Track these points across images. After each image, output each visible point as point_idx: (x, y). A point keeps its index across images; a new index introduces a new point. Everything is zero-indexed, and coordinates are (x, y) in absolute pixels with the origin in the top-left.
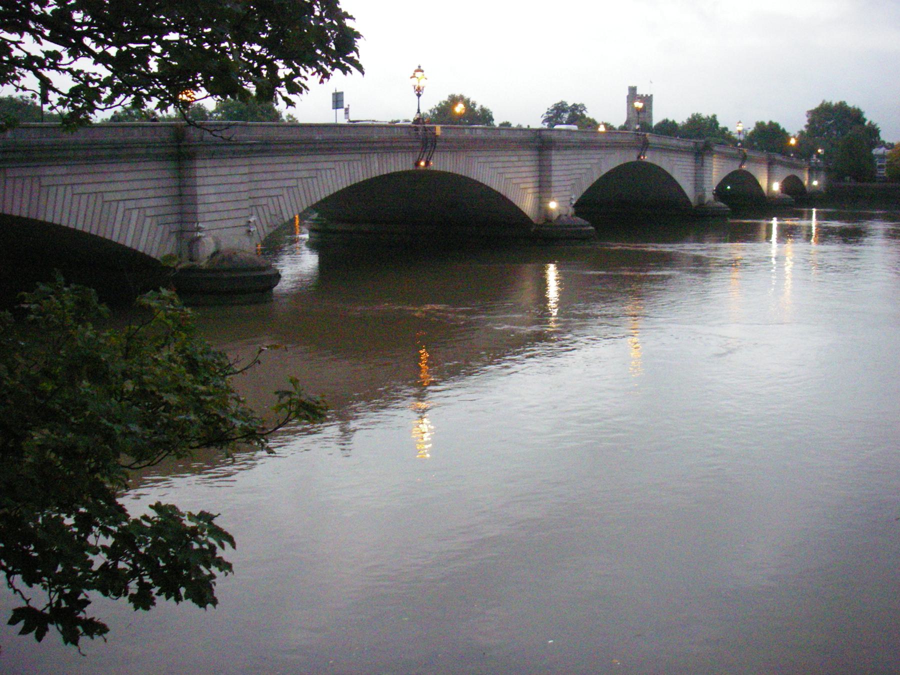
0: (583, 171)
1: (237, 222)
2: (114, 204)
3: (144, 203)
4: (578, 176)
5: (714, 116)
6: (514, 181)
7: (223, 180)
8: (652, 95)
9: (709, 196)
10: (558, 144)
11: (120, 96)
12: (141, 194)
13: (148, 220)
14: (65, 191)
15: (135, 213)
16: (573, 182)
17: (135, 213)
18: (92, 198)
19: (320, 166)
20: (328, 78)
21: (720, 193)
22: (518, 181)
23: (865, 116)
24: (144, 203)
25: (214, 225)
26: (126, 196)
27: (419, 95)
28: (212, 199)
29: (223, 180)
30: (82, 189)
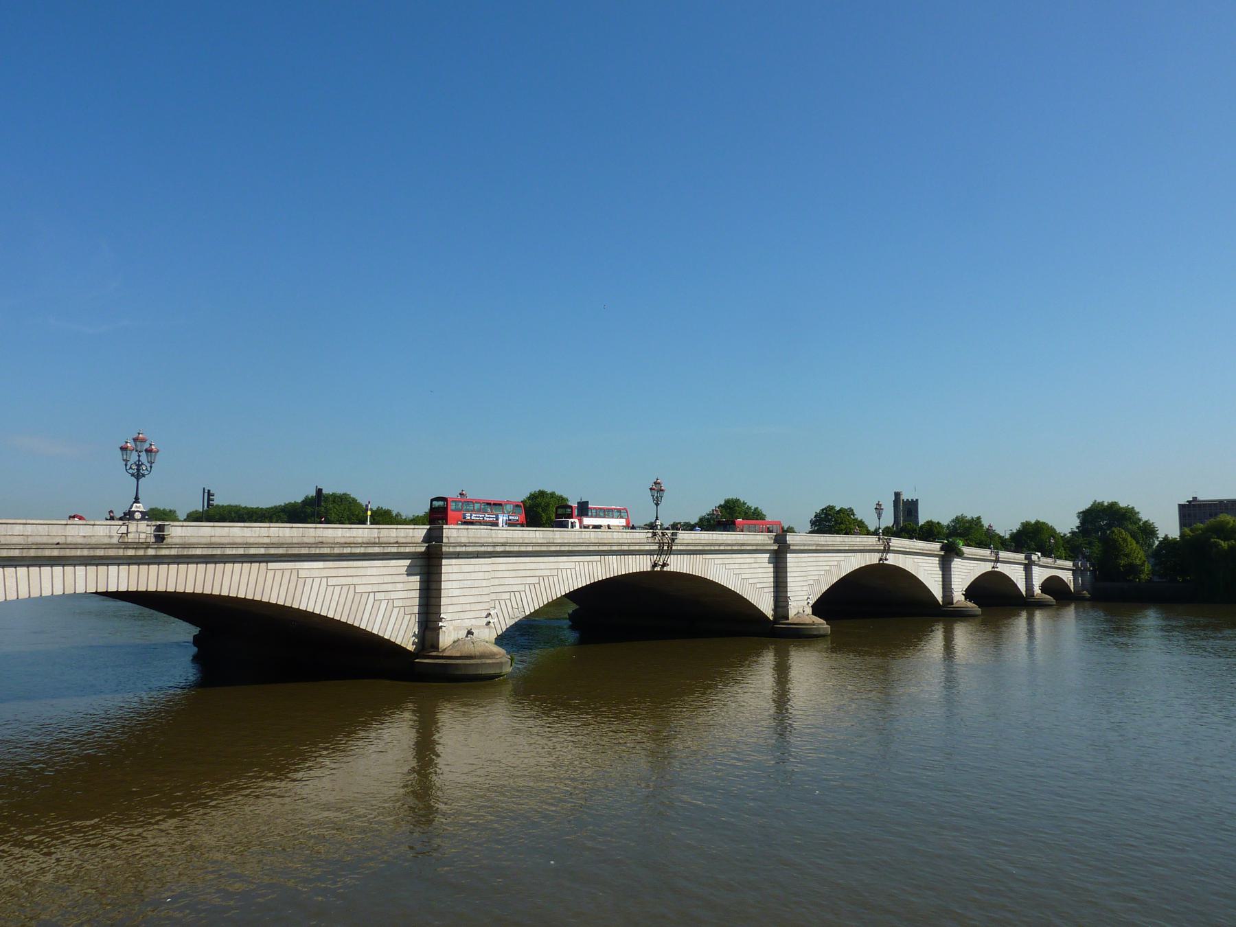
0: (823, 573)
1: (478, 614)
2: (365, 596)
3: (393, 595)
4: (817, 577)
5: (979, 518)
6: (751, 581)
7: (467, 576)
8: (917, 500)
9: (958, 596)
10: (965, 555)
11: (1035, 523)
12: (390, 587)
13: (396, 610)
14: (1031, 632)
15: (384, 604)
16: (811, 582)
17: (384, 604)
18: (338, 589)
19: (561, 565)
20: (1196, 498)
21: (970, 593)
22: (756, 581)
23: (1140, 516)
24: (393, 595)
25: (456, 616)
26: (375, 588)
27: (657, 505)
28: (456, 593)
29: (467, 576)
30: (332, 581)
